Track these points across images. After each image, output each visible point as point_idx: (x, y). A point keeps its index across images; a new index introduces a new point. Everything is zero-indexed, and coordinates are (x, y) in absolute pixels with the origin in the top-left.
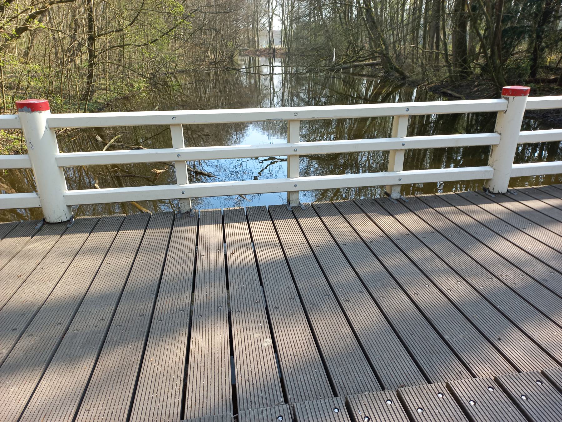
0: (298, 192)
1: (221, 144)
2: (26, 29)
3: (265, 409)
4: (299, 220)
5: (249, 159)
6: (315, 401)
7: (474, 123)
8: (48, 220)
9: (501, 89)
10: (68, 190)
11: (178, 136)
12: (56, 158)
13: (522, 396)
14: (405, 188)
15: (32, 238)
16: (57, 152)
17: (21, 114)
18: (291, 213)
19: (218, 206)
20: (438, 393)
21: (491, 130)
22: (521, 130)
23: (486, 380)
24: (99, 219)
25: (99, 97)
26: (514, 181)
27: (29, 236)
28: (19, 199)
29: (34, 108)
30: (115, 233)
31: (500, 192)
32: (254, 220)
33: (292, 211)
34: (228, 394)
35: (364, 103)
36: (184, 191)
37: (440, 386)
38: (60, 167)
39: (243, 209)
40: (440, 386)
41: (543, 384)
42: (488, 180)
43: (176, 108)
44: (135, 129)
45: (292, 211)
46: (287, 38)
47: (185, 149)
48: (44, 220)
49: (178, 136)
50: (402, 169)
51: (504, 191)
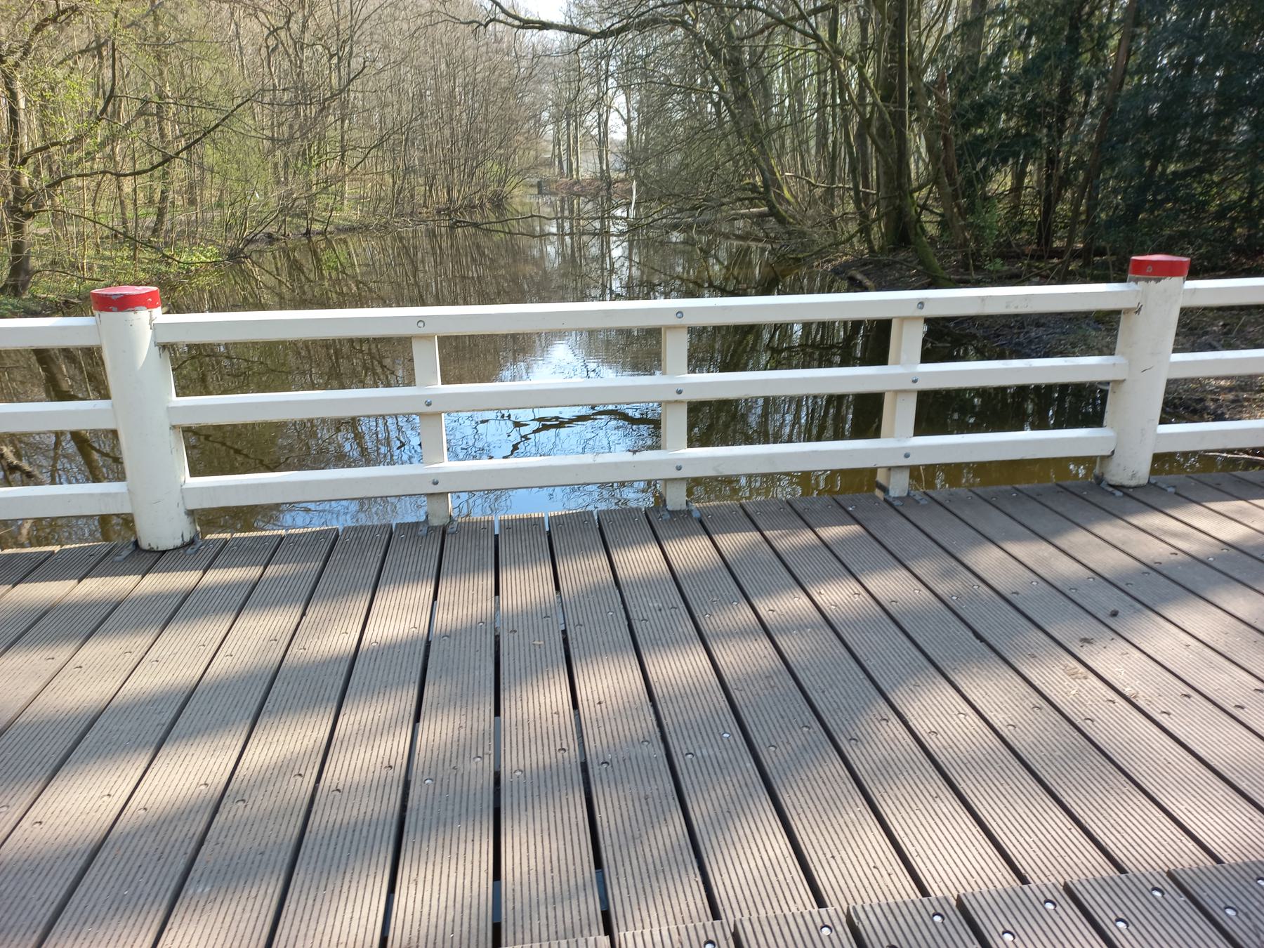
0: (444, 495)
1: (489, 380)
2: (1086, 113)
3: (592, 938)
4: (717, 538)
5: (490, 415)
6: (592, 938)
7: (748, 349)
8: (144, 544)
9: (1128, 261)
10: (191, 476)
11: (428, 360)
12: (168, 408)
13: (1004, 933)
14: (922, 475)
15: (79, 582)
16: (170, 394)
17: (106, 315)
18: (698, 526)
19: (546, 507)
20: (1046, 902)
21: (1112, 353)
22: (1175, 351)
23: (1205, 870)
24: (226, 542)
25: (43, 287)
26: (1161, 461)
27: (194, 568)
28: (214, 488)
29: (125, 304)
30: (199, 573)
31: (154, 546)
32: (671, 537)
33: (701, 522)
34: (482, 915)
35: (848, 291)
36: (908, 451)
37: (835, 909)
38: (174, 427)
39: (492, 522)
40: (835, 909)
41: (1166, 895)
42: (1104, 458)
43: (1113, 275)
44: (269, 348)
45: (701, 522)
46: (634, 156)
47: (441, 388)
48: (136, 543)
49: (428, 360)
50: (911, 431)
51: (1144, 481)
